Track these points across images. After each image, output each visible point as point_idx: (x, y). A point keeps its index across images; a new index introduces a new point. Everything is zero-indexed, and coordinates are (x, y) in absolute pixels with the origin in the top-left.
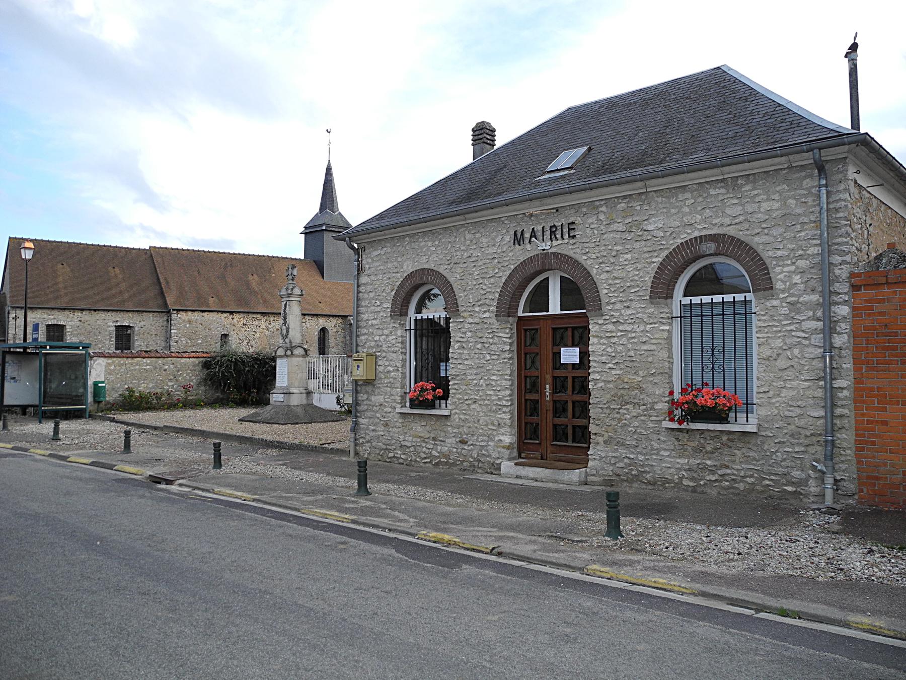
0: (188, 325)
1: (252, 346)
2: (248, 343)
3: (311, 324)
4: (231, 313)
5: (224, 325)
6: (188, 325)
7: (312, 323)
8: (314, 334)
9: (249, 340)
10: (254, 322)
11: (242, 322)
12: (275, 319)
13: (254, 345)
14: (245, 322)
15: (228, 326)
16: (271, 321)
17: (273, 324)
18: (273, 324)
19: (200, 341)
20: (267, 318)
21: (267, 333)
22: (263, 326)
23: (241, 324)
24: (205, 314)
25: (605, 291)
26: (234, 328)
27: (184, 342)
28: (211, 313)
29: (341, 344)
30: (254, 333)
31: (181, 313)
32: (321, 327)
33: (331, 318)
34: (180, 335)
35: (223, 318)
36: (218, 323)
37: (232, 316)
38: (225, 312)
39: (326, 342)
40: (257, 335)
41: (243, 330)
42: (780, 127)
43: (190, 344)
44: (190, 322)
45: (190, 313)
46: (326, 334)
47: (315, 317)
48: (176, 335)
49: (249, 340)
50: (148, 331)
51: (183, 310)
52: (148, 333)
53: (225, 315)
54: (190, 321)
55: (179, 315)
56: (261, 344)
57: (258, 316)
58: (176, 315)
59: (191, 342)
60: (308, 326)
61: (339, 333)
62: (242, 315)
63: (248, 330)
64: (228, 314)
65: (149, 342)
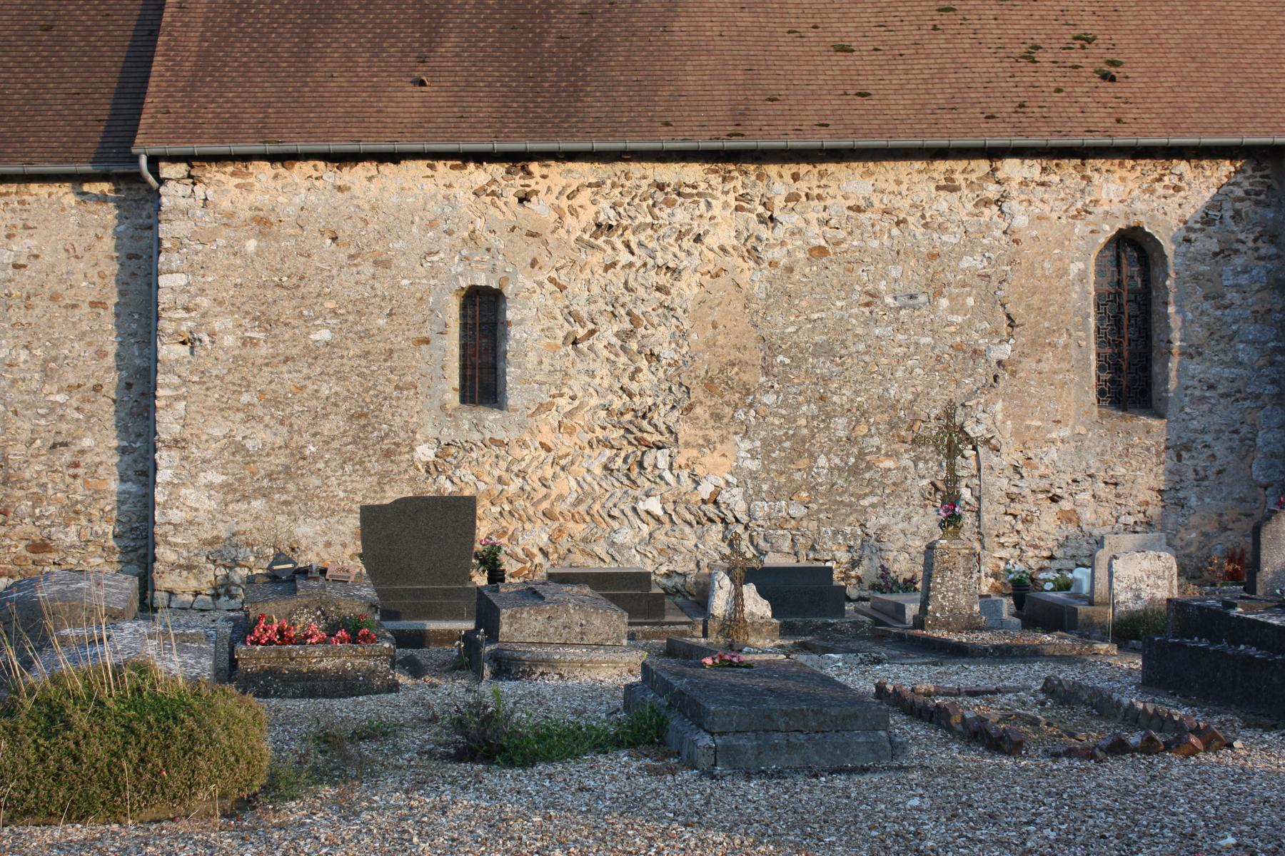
0: (251, 245)
1: (653, 357)
2: (625, 336)
3: (1037, 208)
4: (517, 159)
5: (473, 236)
6: (251, 245)
7: (1051, 203)
8: (1062, 273)
9: (634, 320)
10: (664, 214)
11: (587, 217)
12: (802, 186)
13: (667, 353)
14: (607, 216)
15: (498, 243)
16: (779, 202)
17: (789, 220)
18: (789, 220)
19: (324, 335)
20: (742, 179)
21: (752, 277)
22: (722, 235)
23: (577, 226)
24: (357, 175)
25: (179, 280)
26: (534, 248)
27: (229, 341)
28: (387, 168)
29: (1252, 330)
30: (664, 279)
31: (213, 173)
32: (1109, 231)
33: (1182, 166)
34: (204, 302)
35: (463, 196)
36: (432, 225)
37: (518, 180)
38: (480, 158)
39: (1155, 318)
40: (687, 289)
41: (596, 259)
42: (387, 107)
43: (264, 350)
44: (263, 223)
45: (263, 170)
46: (1156, 271)
47: (1069, 165)
48: (182, 300)
49: (634, 320)
50: (52, 285)
51: (219, 159)
52: (54, 298)
53: (478, 175)
54: (263, 222)
55: (199, 189)
56: (711, 344)
57: (693, 172)
58: (182, 189)
59: (272, 338)
60: (1021, 221)
61: (1238, 261)
62: (584, 171)
63: (625, 257)
64: (498, 170)
65: (56, 344)
